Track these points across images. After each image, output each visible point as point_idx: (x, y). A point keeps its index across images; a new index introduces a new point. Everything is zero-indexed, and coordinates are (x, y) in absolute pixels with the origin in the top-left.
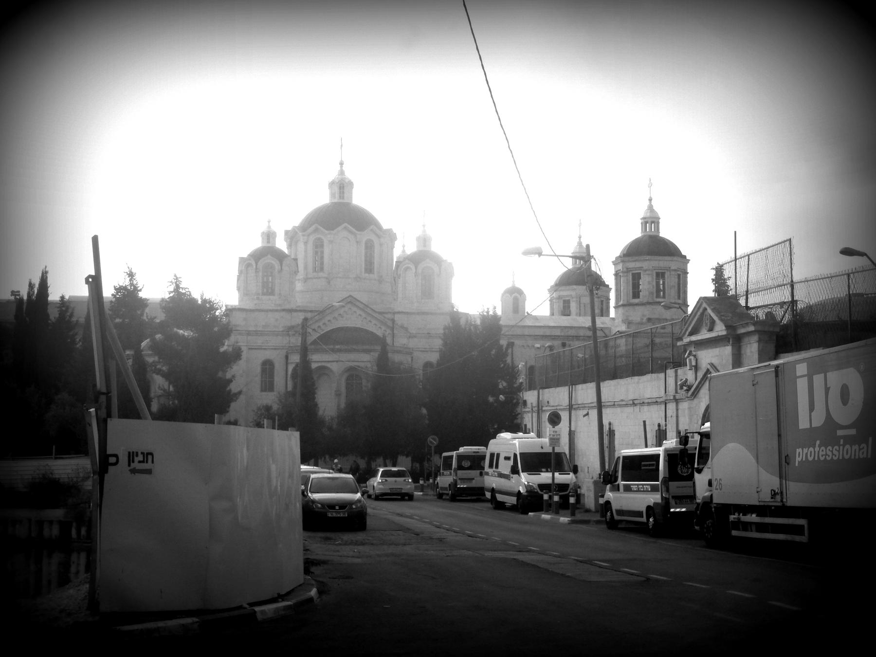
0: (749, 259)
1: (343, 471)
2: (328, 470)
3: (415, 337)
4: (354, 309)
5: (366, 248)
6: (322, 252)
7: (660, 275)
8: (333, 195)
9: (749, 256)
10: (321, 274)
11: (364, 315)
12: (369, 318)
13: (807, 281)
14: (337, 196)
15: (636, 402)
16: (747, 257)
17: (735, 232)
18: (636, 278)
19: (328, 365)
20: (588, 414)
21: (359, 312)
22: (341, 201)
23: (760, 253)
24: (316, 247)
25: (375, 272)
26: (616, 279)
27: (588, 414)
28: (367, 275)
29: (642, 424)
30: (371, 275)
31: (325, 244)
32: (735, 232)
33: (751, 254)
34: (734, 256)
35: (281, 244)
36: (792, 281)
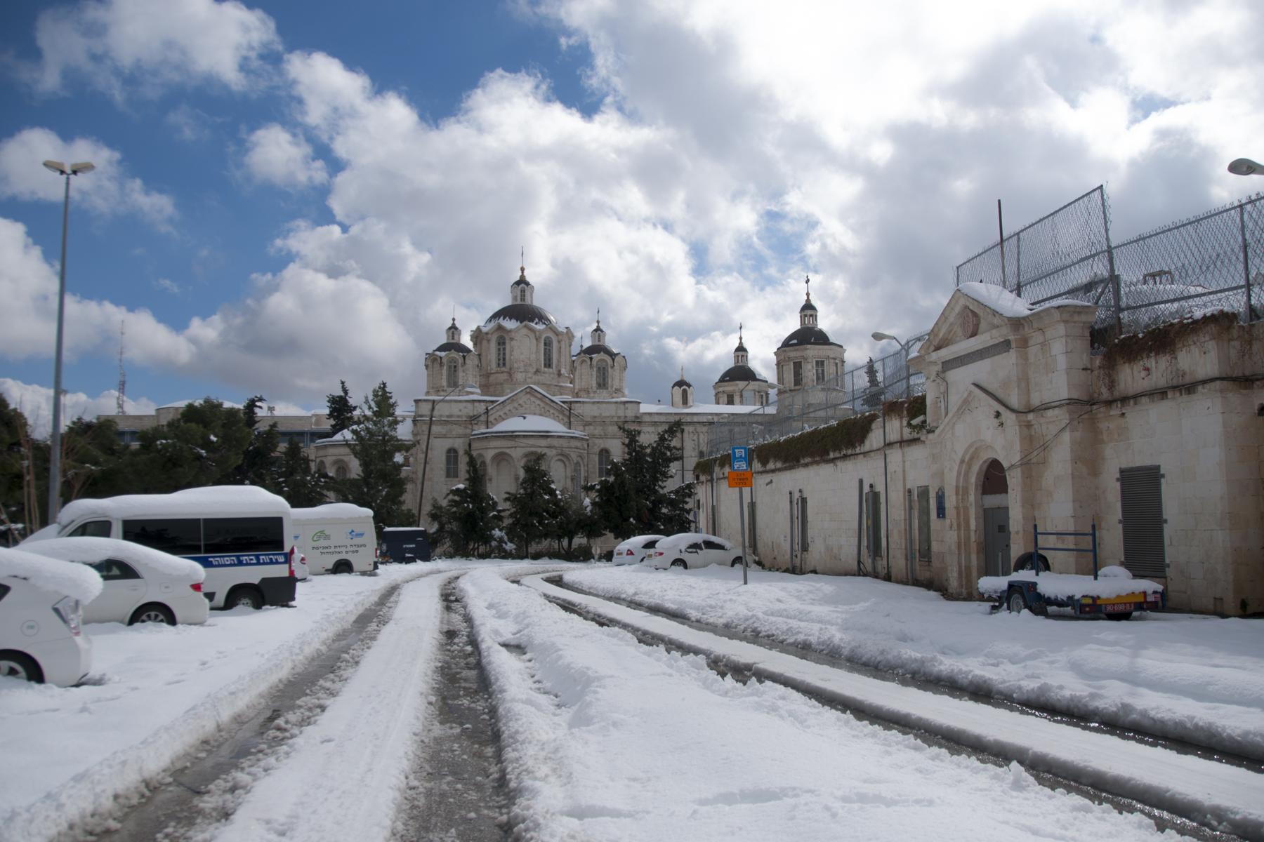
0: (1019, 238)
1: (893, 579)
2: (964, 583)
3: (591, 424)
4: (532, 399)
5: (545, 344)
6: (504, 349)
7: (820, 363)
8: (515, 298)
9: (1018, 234)
10: (503, 369)
11: (542, 405)
12: (547, 408)
13: (1144, 239)
14: (519, 298)
15: (895, 427)
16: (1016, 237)
17: (999, 201)
18: (798, 366)
19: (507, 451)
20: (771, 481)
21: (538, 402)
22: (523, 303)
23: (1039, 225)
24: (499, 344)
25: (554, 367)
26: (778, 368)
27: (771, 481)
28: (546, 369)
29: (857, 485)
30: (550, 370)
31: (507, 341)
32: (999, 201)
33: (1022, 231)
34: (999, 239)
35: (466, 340)
36: (1109, 247)
